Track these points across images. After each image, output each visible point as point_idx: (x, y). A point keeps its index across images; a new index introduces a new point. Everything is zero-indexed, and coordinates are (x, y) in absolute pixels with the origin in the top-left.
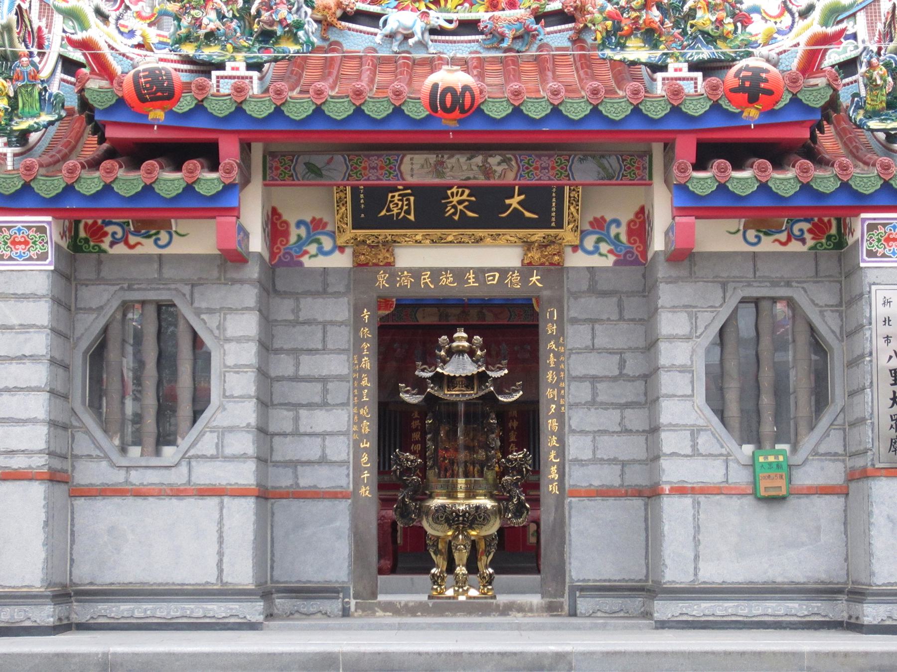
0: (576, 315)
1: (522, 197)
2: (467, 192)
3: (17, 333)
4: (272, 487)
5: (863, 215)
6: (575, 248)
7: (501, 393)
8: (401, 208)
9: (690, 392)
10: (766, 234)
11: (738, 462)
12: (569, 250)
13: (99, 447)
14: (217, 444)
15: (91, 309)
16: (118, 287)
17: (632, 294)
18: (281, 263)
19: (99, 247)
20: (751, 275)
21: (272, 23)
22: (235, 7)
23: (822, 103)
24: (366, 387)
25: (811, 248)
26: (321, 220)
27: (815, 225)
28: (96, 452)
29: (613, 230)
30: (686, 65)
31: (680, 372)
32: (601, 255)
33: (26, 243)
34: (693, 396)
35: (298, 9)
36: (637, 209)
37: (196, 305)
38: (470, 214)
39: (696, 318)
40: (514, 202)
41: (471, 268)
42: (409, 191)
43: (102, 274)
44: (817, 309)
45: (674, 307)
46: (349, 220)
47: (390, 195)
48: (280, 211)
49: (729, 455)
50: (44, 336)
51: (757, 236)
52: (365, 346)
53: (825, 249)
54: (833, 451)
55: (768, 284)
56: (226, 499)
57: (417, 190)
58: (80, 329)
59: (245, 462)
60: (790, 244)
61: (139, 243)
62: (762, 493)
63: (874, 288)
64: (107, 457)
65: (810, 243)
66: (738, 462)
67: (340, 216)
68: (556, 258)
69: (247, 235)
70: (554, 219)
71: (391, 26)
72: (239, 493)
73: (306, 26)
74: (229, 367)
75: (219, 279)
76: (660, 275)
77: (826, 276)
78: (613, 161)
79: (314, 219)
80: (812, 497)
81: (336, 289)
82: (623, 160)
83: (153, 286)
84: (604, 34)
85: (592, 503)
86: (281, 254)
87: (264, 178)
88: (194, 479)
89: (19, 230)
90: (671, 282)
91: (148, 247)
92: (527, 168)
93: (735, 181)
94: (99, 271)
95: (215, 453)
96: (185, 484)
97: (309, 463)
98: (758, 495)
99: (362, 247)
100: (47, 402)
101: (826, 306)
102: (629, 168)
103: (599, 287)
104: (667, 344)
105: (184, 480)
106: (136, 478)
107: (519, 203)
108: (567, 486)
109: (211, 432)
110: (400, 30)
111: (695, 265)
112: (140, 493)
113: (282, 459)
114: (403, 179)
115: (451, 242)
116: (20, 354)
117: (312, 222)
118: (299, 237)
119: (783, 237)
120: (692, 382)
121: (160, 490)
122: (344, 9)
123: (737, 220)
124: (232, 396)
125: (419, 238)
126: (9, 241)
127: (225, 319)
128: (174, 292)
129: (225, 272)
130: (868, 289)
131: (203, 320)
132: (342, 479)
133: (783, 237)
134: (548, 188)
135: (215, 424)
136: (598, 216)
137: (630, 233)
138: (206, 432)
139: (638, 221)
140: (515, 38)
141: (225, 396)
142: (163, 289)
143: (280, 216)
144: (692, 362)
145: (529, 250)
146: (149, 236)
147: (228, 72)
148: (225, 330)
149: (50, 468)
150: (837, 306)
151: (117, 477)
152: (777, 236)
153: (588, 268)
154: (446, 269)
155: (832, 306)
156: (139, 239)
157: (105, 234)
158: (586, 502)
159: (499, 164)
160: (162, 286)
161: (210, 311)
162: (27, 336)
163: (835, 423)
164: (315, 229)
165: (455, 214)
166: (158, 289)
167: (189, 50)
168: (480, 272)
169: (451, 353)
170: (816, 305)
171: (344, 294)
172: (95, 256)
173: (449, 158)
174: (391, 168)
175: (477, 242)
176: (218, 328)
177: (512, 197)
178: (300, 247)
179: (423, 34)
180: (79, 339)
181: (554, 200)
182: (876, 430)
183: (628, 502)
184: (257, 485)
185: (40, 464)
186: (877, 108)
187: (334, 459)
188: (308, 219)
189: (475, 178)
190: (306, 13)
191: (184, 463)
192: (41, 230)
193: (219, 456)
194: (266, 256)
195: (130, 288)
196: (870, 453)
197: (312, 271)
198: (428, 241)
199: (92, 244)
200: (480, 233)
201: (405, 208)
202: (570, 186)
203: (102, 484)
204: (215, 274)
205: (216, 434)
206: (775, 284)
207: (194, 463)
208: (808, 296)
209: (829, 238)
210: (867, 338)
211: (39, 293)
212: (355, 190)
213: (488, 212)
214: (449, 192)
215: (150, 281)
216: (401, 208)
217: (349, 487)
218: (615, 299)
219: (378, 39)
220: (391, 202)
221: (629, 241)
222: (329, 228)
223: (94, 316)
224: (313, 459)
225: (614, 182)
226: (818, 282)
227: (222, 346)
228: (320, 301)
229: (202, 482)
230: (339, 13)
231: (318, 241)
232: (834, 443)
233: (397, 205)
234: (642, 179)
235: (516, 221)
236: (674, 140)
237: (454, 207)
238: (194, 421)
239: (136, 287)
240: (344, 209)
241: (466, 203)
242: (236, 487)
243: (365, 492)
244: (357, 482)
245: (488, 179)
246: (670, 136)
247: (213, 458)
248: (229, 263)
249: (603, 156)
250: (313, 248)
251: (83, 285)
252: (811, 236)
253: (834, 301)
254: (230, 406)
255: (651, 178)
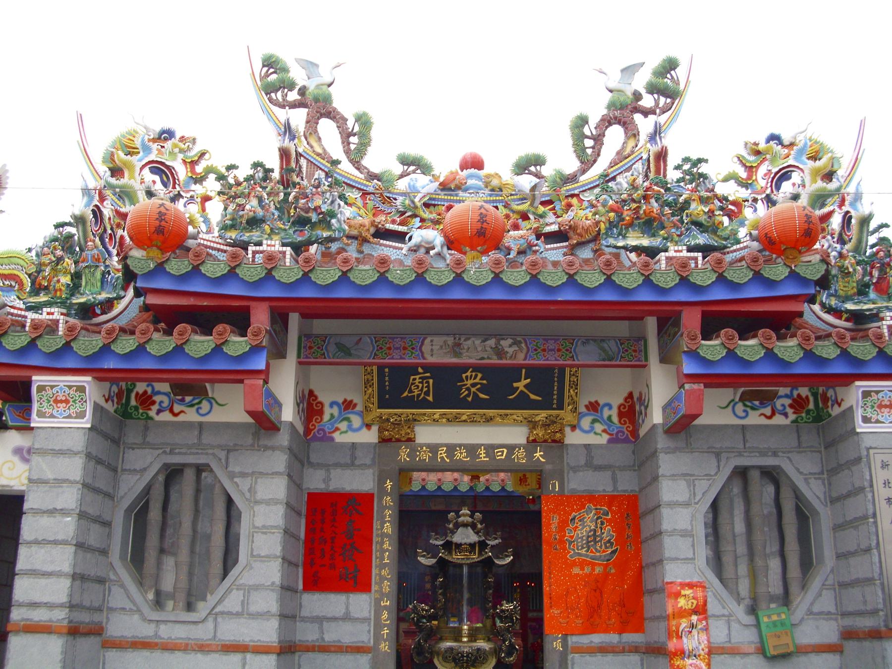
0: (575, 487)
1: (528, 380)
2: (480, 375)
3: (50, 487)
4: (300, 641)
5: (858, 383)
6: (573, 428)
7: (498, 558)
8: (422, 390)
9: (691, 555)
10: (753, 408)
11: (740, 622)
12: (568, 430)
13: (133, 602)
14: (243, 602)
15: (135, 470)
16: (161, 451)
17: (622, 469)
18: (315, 438)
19: (147, 414)
20: (741, 446)
21: (307, 210)
22: (276, 199)
23: (819, 276)
24: (387, 550)
25: (793, 422)
26: (351, 401)
27: (794, 400)
28: (129, 605)
29: (606, 413)
30: (685, 248)
31: (681, 536)
32: (596, 433)
33: (66, 401)
34: (693, 559)
35: (332, 202)
36: (626, 395)
37: (230, 469)
38: (482, 396)
39: (694, 486)
40: (521, 385)
41: (483, 445)
42: (428, 375)
43: (148, 439)
44: (802, 477)
45: (673, 475)
46: (375, 400)
47: (412, 377)
48: (316, 393)
49: (730, 615)
50: (75, 491)
51: (745, 411)
52: (388, 512)
53: (806, 422)
54: (826, 609)
55: (757, 454)
56: (249, 656)
57: (435, 370)
58: (123, 489)
59: (268, 620)
60: (774, 418)
61: (182, 412)
62: (771, 652)
63: (871, 451)
64: (139, 611)
65: (792, 417)
66: (740, 622)
67: (367, 396)
68: (558, 435)
69: (280, 405)
70: (555, 401)
71: (416, 240)
72: (261, 650)
73: (339, 216)
74: (258, 528)
75: (252, 445)
76: (659, 446)
77: (807, 447)
78: (612, 343)
79: (345, 400)
80: (810, 655)
81: (362, 462)
82: (621, 344)
83: (193, 451)
84: (607, 225)
85: (594, 659)
86: (315, 430)
87: (299, 356)
88: (219, 635)
89: (61, 389)
90: (669, 453)
91: (190, 416)
92: (536, 350)
93: (742, 348)
94: (145, 436)
95: (240, 610)
96: (210, 640)
97: (335, 619)
98: (768, 655)
99: (386, 424)
100: (73, 555)
101: (810, 474)
102: (627, 351)
103: (596, 462)
104: (669, 510)
105: (210, 635)
106: (167, 632)
107: (525, 386)
108: (570, 643)
109: (237, 589)
110: (423, 244)
111: (691, 437)
112: (169, 647)
113: (309, 615)
114: (424, 358)
115: (464, 421)
116: (51, 507)
117: (343, 403)
118: (332, 416)
119: (768, 411)
120: (693, 546)
121: (187, 645)
122: (377, 226)
123: (731, 390)
124: (259, 556)
125: (436, 416)
126: (52, 400)
127: (256, 483)
128: (211, 457)
129: (259, 439)
130: (865, 453)
131: (236, 483)
132: (363, 635)
133: (768, 411)
134: (550, 368)
135: (241, 582)
136: (593, 400)
137: (621, 415)
138: (232, 590)
139: (627, 405)
140: (520, 253)
141: (252, 556)
142: (202, 453)
143: (316, 398)
144: (692, 526)
145: (534, 428)
146: (192, 406)
147: (264, 248)
148: (255, 493)
149: (70, 622)
150: (819, 474)
151: (146, 631)
152: (762, 411)
153: (585, 445)
154: (460, 446)
155: (815, 474)
156: (182, 408)
157: (154, 403)
158: (588, 658)
159: (510, 346)
160: (200, 451)
161: (243, 475)
162: (60, 490)
163: (827, 583)
164: (345, 409)
165: (468, 395)
166: (197, 453)
167: (233, 234)
168: (491, 449)
169: (457, 526)
170: (801, 473)
171: (369, 467)
172: (143, 422)
173: (465, 340)
174: (413, 349)
175: (488, 421)
176: (250, 490)
177: (519, 380)
178: (332, 425)
179: (442, 247)
180: (122, 497)
181: (556, 384)
182: (886, 589)
183: (626, 657)
184: (279, 642)
185: (60, 618)
186: (849, 293)
187: (356, 616)
188: (341, 401)
189: (488, 358)
190: (339, 205)
191: (211, 619)
192: (81, 389)
193: (243, 613)
194: (301, 429)
195: (172, 452)
196: (881, 613)
197: (342, 445)
198: (444, 420)
199: (141, 411)
200: (491, 412)
201: (425, 389)
202: (571, 366)
203: (133, 637)
204: (250, 440)
205: (242, 592)
206: (763, 454)
207: (219, 620)
208: (793, 464)
209: (808, 412)
210: (869, 501)
211: (75, 449)
212: (381, 368)
213: (498, 392)
214: (464, 376)
215: (189, 447)
216: (422, 390)
217: (369, 642)
218: (609, 474)
219: (404, 252)
220: (412, 384)
221: (620, 422)
222: (359, 408)
223: (138, 477)
224: (337, 615)
225: (613, 363)
226: (802, 452)
227: (252, 508)
228: (348, 472)
229: (228, 638)
230: (372, 230)
231: (348, 419)
232: (827, 603)
233: (418, 386)
234: (639, 360)
235: (522, 403)
236: (680, 312)
237: (468, 389)
238: (224, 579)
239: (177, 451)
240: (371, 390)
241: (479, 386)
242: (259, 644)
243: (385, 647)
244: (378, 637)
245: (501, 359)
246: (677, 308)
247: (238, 615)
248: (263, 431)
249: (602, 341)
250: (343, 426)
251: (129, 448)
252: (792, 410)
253: (816, 469)
254: (257, 565)
255: (646, 359)
